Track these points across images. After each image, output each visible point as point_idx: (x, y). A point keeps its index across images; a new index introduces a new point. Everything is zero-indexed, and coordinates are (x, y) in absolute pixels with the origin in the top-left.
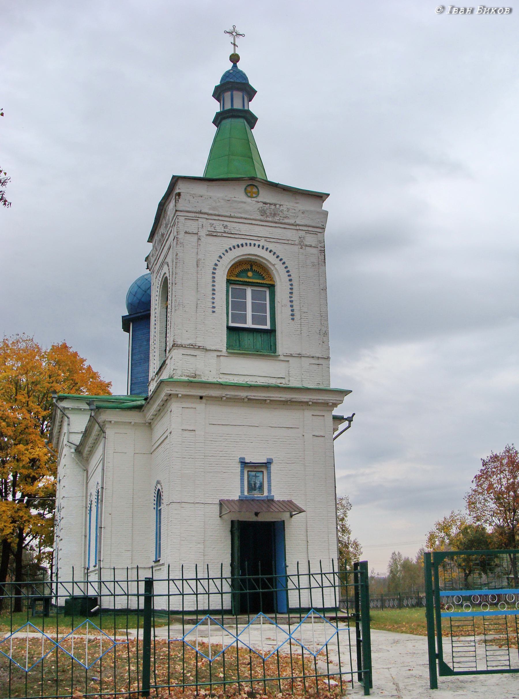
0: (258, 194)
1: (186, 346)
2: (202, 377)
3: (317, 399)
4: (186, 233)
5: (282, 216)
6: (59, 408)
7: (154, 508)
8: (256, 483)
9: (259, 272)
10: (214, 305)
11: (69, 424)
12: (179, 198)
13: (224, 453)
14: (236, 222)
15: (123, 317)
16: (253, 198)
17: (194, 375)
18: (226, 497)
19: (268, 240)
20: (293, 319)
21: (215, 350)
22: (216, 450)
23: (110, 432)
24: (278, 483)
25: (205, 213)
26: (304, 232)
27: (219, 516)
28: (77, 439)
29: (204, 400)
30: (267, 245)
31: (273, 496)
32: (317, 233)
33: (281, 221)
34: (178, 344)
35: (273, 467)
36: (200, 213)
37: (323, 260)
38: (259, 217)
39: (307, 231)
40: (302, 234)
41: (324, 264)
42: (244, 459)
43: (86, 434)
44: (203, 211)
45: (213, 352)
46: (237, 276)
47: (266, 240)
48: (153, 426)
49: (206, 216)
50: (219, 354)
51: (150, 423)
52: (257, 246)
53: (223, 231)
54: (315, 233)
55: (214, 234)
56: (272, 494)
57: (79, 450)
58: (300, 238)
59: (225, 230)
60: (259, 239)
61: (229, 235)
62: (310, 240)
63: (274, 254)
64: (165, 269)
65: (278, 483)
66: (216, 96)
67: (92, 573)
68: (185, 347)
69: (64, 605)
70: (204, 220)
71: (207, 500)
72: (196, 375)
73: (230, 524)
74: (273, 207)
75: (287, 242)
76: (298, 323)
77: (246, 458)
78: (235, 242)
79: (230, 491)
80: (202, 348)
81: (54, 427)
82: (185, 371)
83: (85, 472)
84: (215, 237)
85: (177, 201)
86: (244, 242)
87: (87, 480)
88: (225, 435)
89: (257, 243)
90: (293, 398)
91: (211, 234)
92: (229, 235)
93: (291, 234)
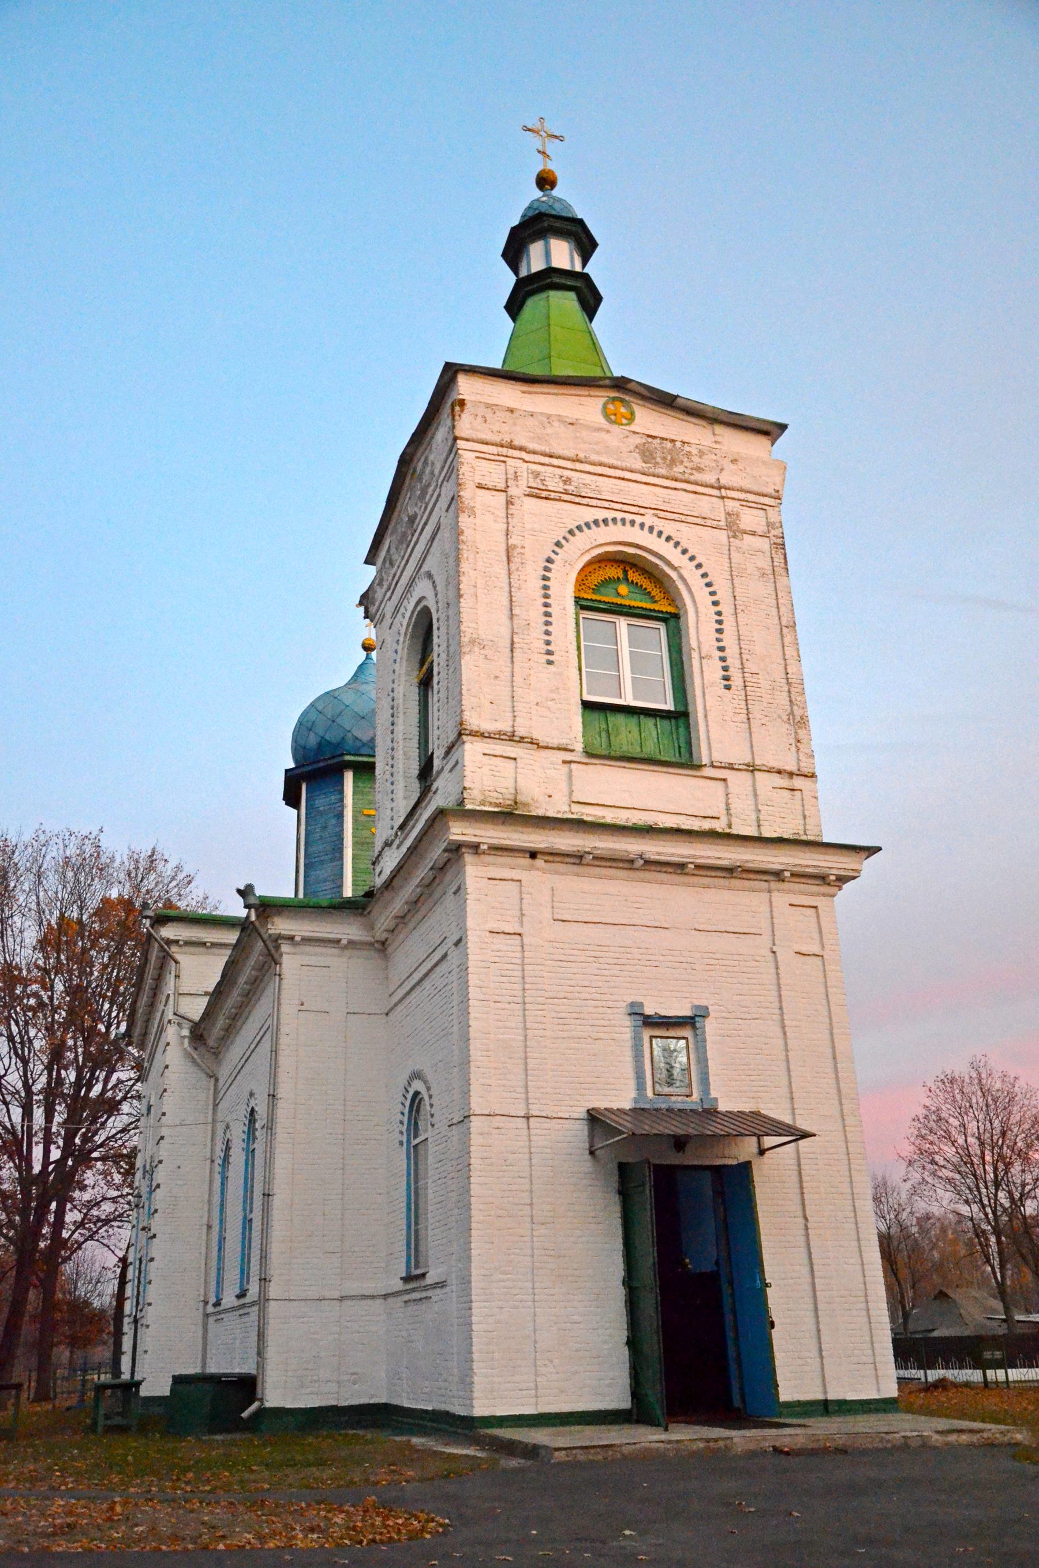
0: (631, 418)
1: (492, 735)
2: (532, 808)
3: (802, 866)
4: (480, 487)
5: (687, 464)
6: (156, 940)
7: (401, 1143)
8: (672, 1067)
9: (641, 586)
10: (549, 648)
11: (177, 976)
12: (462, 411)
13: (594, 990)
14: (589, 473)
15: (287, 771)
16: (622, 425)
17: (512, 803)
18: (601, 1103)
19: (662, 514)
20: (728, 688)
21: (559, 749)
22: (572, 983)
23: (290, 961)
24: (725, 1067)
25: (521, 449)
26: (737, 504)
27: (588, 1152)
28: (195, 1009)
29: (539, 862)
30: (659, 525)
31: (716, 1099)
32: (764, 507)
33: (687, 475)
34: (472, 731)
35: (710, 1027)
36: (512, 447)
37: (783, 565)
38: (638, 464)
39: (743, 500)
40: (731, 505)
41: (784, 574)
42: (641, 1005)
43: (218, 995)
44: (516, 443)
45: (552, 751)
46: (594, 591)
47: (656, 516)
48: (390, 950)
49: (524, 455)
50: (568, 757)
51: (383, 943)
52: (637, 526)
53: (562, 490)
54: (760, 506)
55: (543, 496)
56: (713, 1094)
57: (198, 1034)
58: (728, 514)
59: (566, 487)
60: (642, 511)
61: (577, 500)
62: (750, 519)
63: (677, 544)
64: (423, 588)
65: (725, 1067)
66: (288, 775)
67: (228, 1315)
68: (490, 737)
69: (168, 1394)
70: (519, 463)
71: (557, 1108)
72: (516, 803)
73: (616, 1172)
74: (669, 445)
75: (703, 522)
76: (740, 698)
77: (645, 1004)
78: (590, 514)
79: (613, 1087)
80: (529, 740)
81: (141, 994)
82: (491, 794)
83: (213, 1080)
84: (544, 501)
85: (457, 417)
86: (610, 515)
87: (215, 1100)
88: (591, 947)
89: (639, 519)
90: (747, 861)
91: (535, 494)
92: (577, 500)
93: (708, 506)
